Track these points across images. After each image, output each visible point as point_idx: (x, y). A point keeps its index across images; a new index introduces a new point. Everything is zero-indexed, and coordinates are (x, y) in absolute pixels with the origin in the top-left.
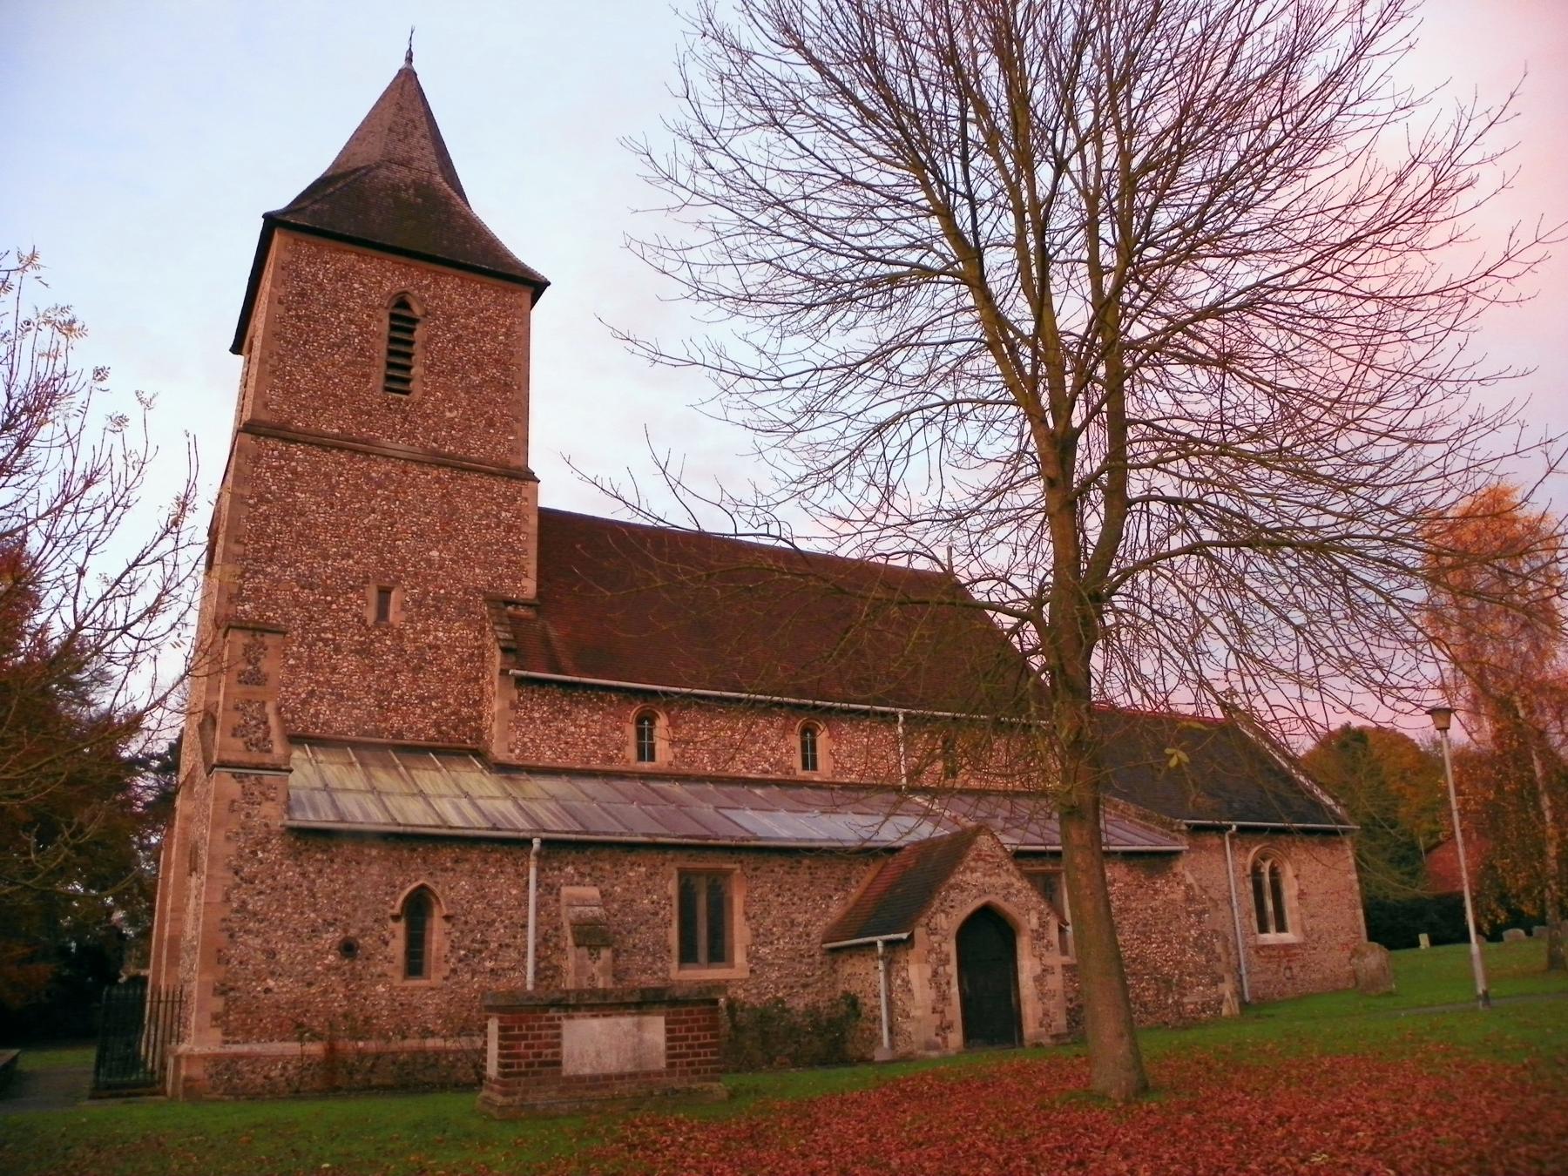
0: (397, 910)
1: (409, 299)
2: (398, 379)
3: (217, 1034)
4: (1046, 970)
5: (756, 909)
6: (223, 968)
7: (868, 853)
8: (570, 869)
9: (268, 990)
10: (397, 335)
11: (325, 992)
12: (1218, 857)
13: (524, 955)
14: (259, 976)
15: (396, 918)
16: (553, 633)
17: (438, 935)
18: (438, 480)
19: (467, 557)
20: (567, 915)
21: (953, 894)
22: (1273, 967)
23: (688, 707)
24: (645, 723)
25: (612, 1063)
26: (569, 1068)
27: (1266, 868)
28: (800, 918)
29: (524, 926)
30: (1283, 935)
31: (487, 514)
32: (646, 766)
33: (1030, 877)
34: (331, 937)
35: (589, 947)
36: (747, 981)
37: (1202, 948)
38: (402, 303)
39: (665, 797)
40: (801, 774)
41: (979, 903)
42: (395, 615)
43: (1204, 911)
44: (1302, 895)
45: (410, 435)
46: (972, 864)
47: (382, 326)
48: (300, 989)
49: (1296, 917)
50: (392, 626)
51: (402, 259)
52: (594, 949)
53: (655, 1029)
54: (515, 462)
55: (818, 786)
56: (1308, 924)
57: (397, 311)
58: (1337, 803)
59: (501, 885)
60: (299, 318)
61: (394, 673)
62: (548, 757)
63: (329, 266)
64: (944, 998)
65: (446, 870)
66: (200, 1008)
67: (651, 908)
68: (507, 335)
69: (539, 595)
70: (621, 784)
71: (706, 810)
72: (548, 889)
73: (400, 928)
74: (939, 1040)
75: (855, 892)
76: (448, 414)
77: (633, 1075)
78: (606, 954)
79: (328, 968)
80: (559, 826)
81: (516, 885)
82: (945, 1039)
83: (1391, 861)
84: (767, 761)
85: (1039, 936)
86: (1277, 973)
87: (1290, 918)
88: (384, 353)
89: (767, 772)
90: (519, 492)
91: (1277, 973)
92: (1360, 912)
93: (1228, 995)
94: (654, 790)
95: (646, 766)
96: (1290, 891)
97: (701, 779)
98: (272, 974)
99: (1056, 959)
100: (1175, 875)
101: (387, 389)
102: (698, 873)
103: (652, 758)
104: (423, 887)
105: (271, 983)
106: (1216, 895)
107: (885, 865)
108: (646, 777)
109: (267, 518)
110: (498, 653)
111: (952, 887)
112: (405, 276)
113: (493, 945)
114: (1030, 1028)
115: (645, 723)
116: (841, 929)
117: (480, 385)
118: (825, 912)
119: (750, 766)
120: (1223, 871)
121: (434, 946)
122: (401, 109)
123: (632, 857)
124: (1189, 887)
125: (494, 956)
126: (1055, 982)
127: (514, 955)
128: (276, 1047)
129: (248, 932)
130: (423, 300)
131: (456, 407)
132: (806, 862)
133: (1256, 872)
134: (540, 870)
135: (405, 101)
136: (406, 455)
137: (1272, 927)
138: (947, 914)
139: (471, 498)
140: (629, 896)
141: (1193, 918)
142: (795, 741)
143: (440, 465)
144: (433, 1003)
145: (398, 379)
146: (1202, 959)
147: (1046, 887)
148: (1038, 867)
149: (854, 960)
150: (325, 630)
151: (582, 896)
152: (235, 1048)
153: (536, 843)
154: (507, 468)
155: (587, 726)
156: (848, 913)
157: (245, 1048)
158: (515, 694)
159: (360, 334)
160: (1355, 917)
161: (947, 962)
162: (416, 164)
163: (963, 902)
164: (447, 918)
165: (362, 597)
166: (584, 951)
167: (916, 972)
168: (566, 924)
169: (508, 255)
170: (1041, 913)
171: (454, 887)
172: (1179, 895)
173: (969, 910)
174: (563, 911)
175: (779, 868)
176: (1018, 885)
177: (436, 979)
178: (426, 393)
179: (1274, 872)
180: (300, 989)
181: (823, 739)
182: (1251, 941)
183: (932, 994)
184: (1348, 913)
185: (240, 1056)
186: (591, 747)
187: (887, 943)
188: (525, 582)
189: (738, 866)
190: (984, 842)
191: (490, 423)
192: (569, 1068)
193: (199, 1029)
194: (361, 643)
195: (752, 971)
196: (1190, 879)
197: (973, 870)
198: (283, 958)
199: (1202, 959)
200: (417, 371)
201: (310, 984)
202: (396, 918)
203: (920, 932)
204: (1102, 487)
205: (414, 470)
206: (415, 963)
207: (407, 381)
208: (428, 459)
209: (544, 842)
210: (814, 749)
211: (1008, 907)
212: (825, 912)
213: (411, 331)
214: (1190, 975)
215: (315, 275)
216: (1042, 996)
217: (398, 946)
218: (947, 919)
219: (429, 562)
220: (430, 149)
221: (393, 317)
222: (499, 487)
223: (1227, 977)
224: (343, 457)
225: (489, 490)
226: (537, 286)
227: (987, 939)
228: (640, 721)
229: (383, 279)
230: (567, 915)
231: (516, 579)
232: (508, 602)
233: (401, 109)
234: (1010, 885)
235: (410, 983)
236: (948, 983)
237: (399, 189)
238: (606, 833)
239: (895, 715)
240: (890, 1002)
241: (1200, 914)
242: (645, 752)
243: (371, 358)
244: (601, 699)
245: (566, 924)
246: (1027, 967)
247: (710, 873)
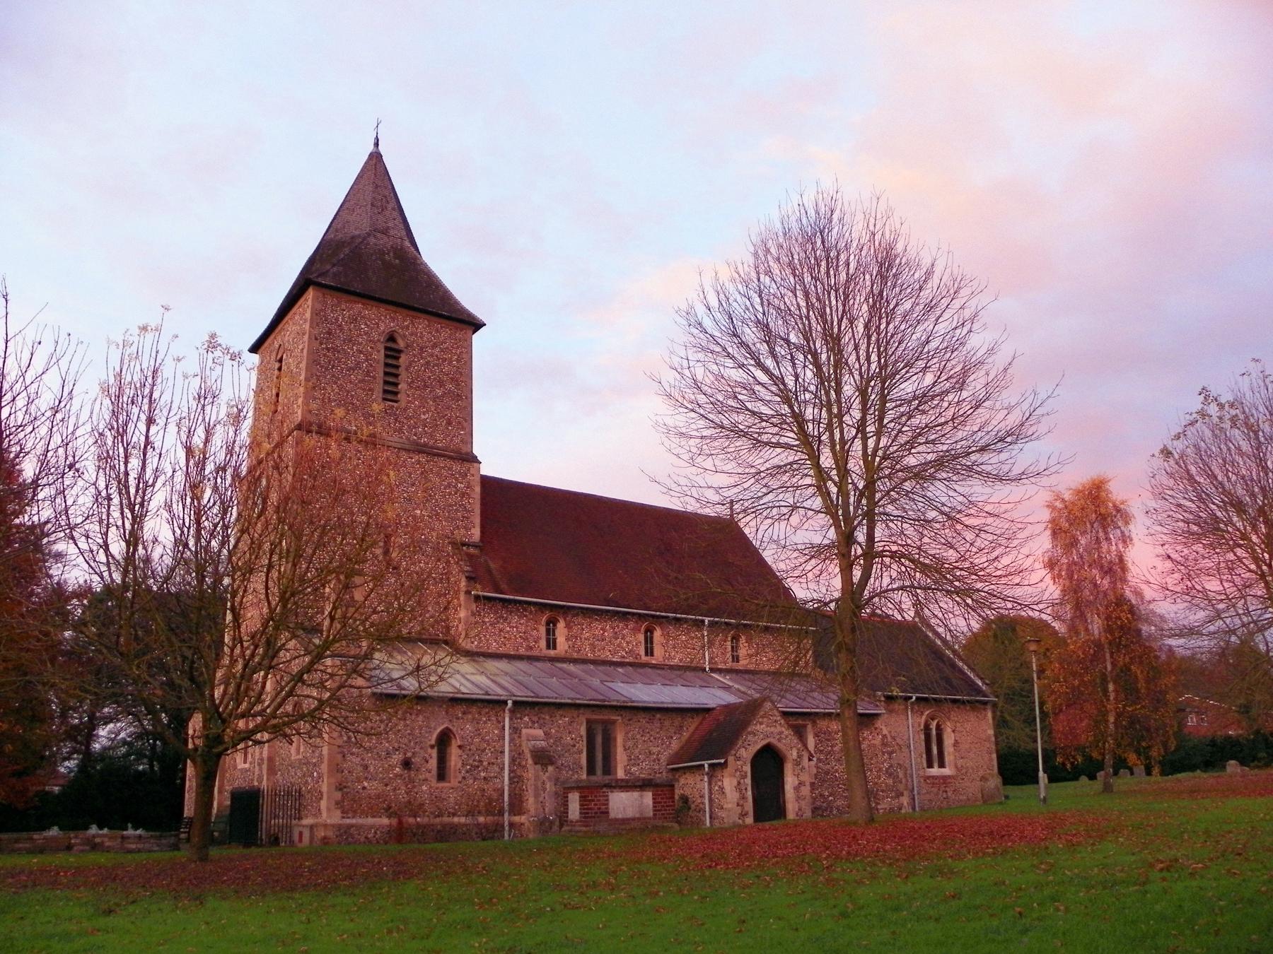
0: (433, 742)
1: (396, 335)
2: (390, 393)
3: (338, 813)
4: (801, 784)
5: (630, 744)
6: (339, 775)
7: (701, 711)
8: (526, 719)
9: (364, 788)
10: (390, 361)
11: (395, 790)
12: (903, 717)
13: (503, 769)
14: (359, 780)
15: (432, 747)
16: (492, 566)
17: (455, 757)
18: (419, 462)
19: (438, 514)
20: (526, 747)
22: (935, 790)
23: (577, 615)
25: (630, 813)
26: (612, 815)
27: (933, 725)
28: (655, 750)
29: (502, 752)
30: (942, 770)
31: (449, 485)
32: (552, 653)
33: (791, 726)
34: (397, 758)
38: (392, 338)
39: (571, 675)
40: (644, 659)
41: (764, 742)
43: (892, 752)
44: (956, 744)
45: (400, 431)
47: (380, 356)
48: (381, 787)
49: (952, 758)
51: (391, 307)
52: (544, 766)
53: (648, 798)
54: (465, 449)
55: (654, 667)
56: (960, 762)
57: (389, 345)
58: (984, 683)
59: (490, 729)
60: (328, 349)
62: (494, 647)
63: (345, 311)
64: (744, 798)
66: (329, 798)
67: (572, 742)
68: (458, 361)
69: (481, 540)
70: (539, 664)
71: (596, 682)
72: (515, 730)
73: (434, 753)
75: (686, 735)
77: (639, 819)
78: (550, 768)
79: (396, 775)
80: (522, 694)
81: (497, 728)
83: (1025, 721)
85: (797, 763)
86: (937, 794)
87: (948, 758)
88: (382, 374)
91: (937, 794)
92: (994, 756)
94: (560, 669)
95: (552, 653)
96: (948, 740)
97: (584, 661)
98: (366, 778)
99: (806, 778)
101: (384, 399)
102: (596, 721)
103: (555, 648)
104: (447, 728)
106: (901, 742)
107: (704, 719)
108: (552, 660)
110: (464, 579)
112: (393, 319)
114: (791, 815)
116: (676, 758)
117: (443, 396)
118: (668, 747)
119: (614, 653)
120: (902, 728)
121: (453, 763)
122: (377, 187)
123: (561, 712)
124: (885, 736)
125: (486, 769)
126: (806, 791)
127: (497, 769)
128: (370, 821)
129: (352, 754)
130: (405, 336)
131: (428, 412)
133: (927, 728)
134: (511, 719)
135: (375, 180)
137: (936, 765)
139: (439, 475)
141: (886, 756)
142: (641, 637)
143: (420, 452)
144: (452, 797)
145: (390, 393)
147: (800, 733)
148: (798, 721)
149: (687, 775)
151: (534, 735)
152: (348, 821)
153: (510, 702)
156: (682, 748)
157: (354, 821)
158: (474, 606)
159: (367, 360)
160: (991, 760)
161: (745, 777)
162: (392, 232)
163: (756, 742)
164: (460, 747)
166: (539, 767)
167: (728, 783)
168: (527, 752)
169: (457, 303)
171: (464, 728)
172: (878, 741)
173: (758, 747)
174: (524, 744)
175: (643, 719)
176: (786, 733)
177: (454, 782)
178: (409, 402)
179: (938, 727)
180: (381, 787)
181: (658, 634)
182: (921, 773)
183: (737, 795)
184: (986, 757)
185: (352, 826)
186: (519, 640)
187: (710, 765)
188: (473, 531)
190: (768, 705)
191: (449, 423)
192: (612, 815)
193: (329, 810)
196: (885, 732)
197: (761, 724)
198: (371, 769)
199: (890, 781)
200: (403, 386)
202: (432, 747)
203: (731, 759)
204: (859, 544)
205: (404, 455)
206: (442, 775)
207: (396, 393)
208: (412, 448)
209: (515, 703)
210: (652, 643)
211: (780, 745)
212: (668, 747)
213: (398, 358)
215: (337, 319)
216: (798, 798)
217: (433, 763)
218: (746, 752)
219: (414, 517)
220: (399, 219)
221: (386, 348)
222: (456, 467)
225: (450, 469)
226: (477, 325)
227: (768, 765)
228: (548, 624)
229: (376, 323)
230: (526, 747)
231: (467, 529)
232: (464, 544)
233: (377, 187)
235: (441, 785)
237: (384, 254)
239: (703, 621)
240: (711, 800)
241: (890, 753)
242: (551, 644)
243: (374, 377)
244: (525, 610)
245: (527, 752)
246: (790, 781)
247: (604, 722)
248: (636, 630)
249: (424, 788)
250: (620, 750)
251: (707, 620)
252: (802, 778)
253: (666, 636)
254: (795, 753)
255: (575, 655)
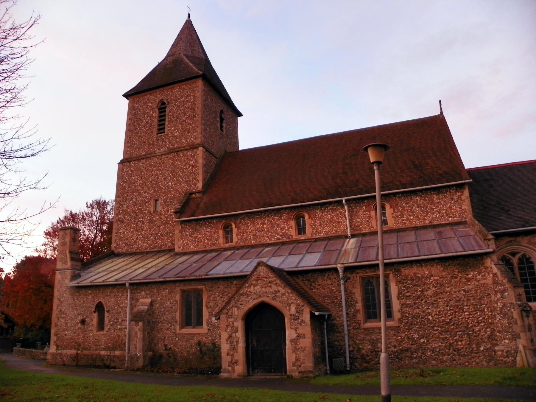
8: (143, 293)
9: (66, 335)
11: (78, 335)
14: (64, 331)
15: (95, 312)
21: (242, 298)
23: (244, 218)
24: (227, 230)
34: (80, 318)
35: (135, 321)
36: (207, 334)
37: (505, 314)
41: (256, 302)
42: (159, 208)
43: (504, 291)
46: (254, 282)
50: (158, 212)
61: (159, 227)
62: (192, 248)
65: (107, 296)
67: (170, 305)
73: (95, 315)
74: (230, 368)
76: (176, 134)
79: (79, 328)
82: (233, 368)
84: (278, 234)
89: (279, 239)
90: (196, 153)
93: (521, 348)
100: (486, 268)
105: (66, 332)
109: (125, 188)
111: (242, 294)
113: (120, 320)
115: (227, 230)
125: (121, 324)
132: (235, 282)
136: (161, 154)
138: (238, 308)
139: (181, 161)
140: (162, 301)
141: (499, 295)
142: (292, 223)
145: (161, 129)
146: (505, 322)
150: (140, 218)
154: (193, 145)
155: (205, 234)
163: (248, 302)
165: (150, 204)
170: (298, 305)
176: (282, 291)
177: (105, 332)
186: (206, 241)
189: (203, 287)
194: (149, 219)
195: (209, 330)
197: (255, 285)
198: (69, 325)
199: (505, 322)
201: (75, 333)
206: (101, 326)
211: (276, 303)
214: (499, 332)
217: (95, 321)
219: (168, 187)
223: (522, 335)
224: (144, 161)
234: (276, 292)
236: (237, 342)
238: (169, 278)
244: (210, 223)
247: (195, 290)
248: (287, 221)
249: (91, 335)
250: (204, 308)
251: (344, 199)
252: (301, 331)
253: (394, 207)
254: (293, 309)
255: (242, 244)
